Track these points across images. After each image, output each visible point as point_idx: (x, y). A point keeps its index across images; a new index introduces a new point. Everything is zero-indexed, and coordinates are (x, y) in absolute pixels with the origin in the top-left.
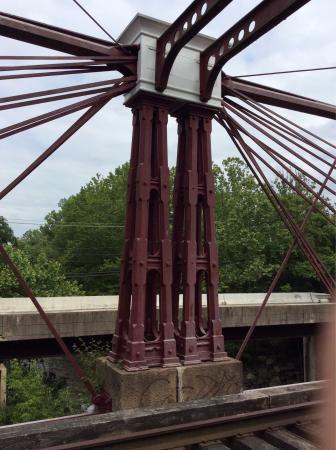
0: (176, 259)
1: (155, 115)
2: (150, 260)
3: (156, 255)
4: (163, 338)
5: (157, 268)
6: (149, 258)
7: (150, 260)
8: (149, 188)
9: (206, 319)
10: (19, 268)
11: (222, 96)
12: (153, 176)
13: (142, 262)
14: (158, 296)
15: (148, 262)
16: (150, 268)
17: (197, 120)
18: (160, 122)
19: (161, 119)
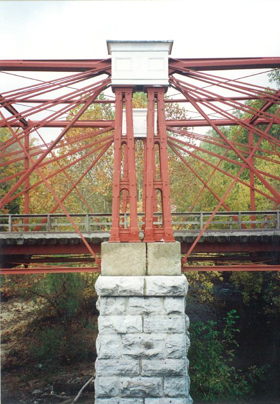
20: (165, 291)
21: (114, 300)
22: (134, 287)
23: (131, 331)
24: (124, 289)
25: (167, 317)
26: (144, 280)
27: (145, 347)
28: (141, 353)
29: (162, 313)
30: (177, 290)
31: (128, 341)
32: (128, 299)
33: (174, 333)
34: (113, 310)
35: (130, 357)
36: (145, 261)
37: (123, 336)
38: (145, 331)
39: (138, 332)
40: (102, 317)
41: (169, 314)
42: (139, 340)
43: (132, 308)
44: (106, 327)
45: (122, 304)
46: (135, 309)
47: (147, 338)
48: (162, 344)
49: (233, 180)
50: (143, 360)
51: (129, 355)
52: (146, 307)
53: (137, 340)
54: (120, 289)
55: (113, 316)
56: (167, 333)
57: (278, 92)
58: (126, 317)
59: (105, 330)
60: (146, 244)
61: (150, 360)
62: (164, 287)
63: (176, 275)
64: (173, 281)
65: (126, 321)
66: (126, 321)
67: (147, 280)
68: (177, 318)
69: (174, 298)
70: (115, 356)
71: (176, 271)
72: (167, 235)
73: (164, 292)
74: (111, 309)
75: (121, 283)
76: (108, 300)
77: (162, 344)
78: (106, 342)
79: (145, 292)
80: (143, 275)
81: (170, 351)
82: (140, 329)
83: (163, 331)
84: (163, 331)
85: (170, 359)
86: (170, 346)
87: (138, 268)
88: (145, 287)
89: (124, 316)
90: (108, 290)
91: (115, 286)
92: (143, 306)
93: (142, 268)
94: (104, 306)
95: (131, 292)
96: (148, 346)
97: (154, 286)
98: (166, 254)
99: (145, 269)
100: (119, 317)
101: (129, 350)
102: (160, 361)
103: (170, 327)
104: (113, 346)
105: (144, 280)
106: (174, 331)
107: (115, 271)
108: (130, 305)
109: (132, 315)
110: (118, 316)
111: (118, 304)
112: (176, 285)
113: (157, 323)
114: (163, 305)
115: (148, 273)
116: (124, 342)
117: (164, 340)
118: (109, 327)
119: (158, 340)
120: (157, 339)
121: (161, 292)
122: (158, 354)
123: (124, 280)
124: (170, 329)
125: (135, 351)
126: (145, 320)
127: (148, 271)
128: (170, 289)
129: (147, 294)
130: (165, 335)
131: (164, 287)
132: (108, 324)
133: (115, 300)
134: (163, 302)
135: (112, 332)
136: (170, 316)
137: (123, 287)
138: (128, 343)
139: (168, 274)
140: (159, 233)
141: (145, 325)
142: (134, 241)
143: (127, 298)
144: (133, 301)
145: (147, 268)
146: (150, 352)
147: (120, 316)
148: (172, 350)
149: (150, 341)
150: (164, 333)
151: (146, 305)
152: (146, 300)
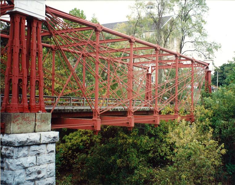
0: (19, 87)
1: (21, 20)
2: (19, 75)
3: (21, 73)
4: (24, 103)
5: (21, 78)
6: (19, 74)
7: (19, 75)
8: (19, 48)
9: (139, 145)
10: (85, 95)
11: (46, 15)
12: (20, 43)
13: (17, 75)
14: (26, 21)
15: (19, 76)
16: (20, 78)
17: (36, 23)
18: (22, 23)
19: (23, 22)
20: (50, 140)
21: (22, 149)
22: (36, 139)
23: (31, 165)
24: (31, 141)
25: (48, 155)
26: (40, 134)
27: (38, 173)
28: (36, 178)
29: (46, 153)
30: (55, 138)
31: (30, 172)
32: (30, 147)
33: (50, 163)
34: (22, 154)
35: (30, 181)
36: (34, 124)
37: (26, 169)
38: (37, 164)
39: (34, 165)
40: (16, 159)
41: (48, 153)
42: (35, 170)
43: (31, 152)
44: (17, 165)
45: (26, 150)
46: (33, 152)
47: (38, 168)
48: (45, 170)
49: (164, 110)
50: (36, 181)
51: (29, 180)
52: (39, 150)
53: (34, 170)
54: (29, 141)
55: (21, 158)
56: (48, 163)
57: (60, 30)
58: (28, 158)
59: (17, 167)
60: (35, 114)
61: (39, 180)
62: (50, 138)
63: (49, 131)
64: (54, 134)
65: (28, 160)
66: (28, 160)
67: (41, 134)
68: (52, 155)
69: (52, 144)
70: (22, 182)
71: (49, 129)
72: (42, 109)
73: (49, 140)
74: (21, 154)
75: (29, 137)
76: (19, 149)
77: (45, 170)
78: (18, 174)
79: (40, 142)
80: (33, 132)
81: (48, 173)
82: (35, 164)
83: (46, 163)
84: (46, 163)
85: (49, 178)
86: (49, 171)
87: (31, 128)
88: (40, 139)
89: (27, 157)
90: (23, 142)
91: (26, 139)
92: (38, 150)
93: (32, 130)
94: (17, 153)
95: (34, 142)
96: (39, 173)
97: (45, 138)
98: (44, 121)
99: (34, 129)
100: (25, 158)
101: (29, 177)
102: (44, 180)
103: (49, 160)
104: (22, 176)
105: (40, 134)
106: (51, 162)
107: (19, 131)
108: (31, 150)
109: (31, 156)
110: (24, 158)
111: (24, 151)
112: (56, 136)
113: (43, 159)
114: (46, 148)
115: (36, 131)
116: (27, 173)
117: (46, 168)
118: (20, 165)
119: (44, 168)
120: (43, 168)
121: (47, 141)
122: (44, 176)
123: (30, 135)
124: (49, 161)
125: (33, 177)
126: (37, 158)
127: (36, 129)
128: (52, 138)
129: (41, 143)
130: (47, 165)
131: (50, 138)
132: (20, 163)
133: (23, 148)
134: (47, 146)
135: (20, 168)
136: (50, 154)
137: (30, 140)
138: (29, 173)
139: (45, 131)
140: (38, 107)
141: (37, 161)
142: (27, 112)
143: (29, 146)
144: (33, 148)
145: (35, 128)
146: (40, 176)
147: (25, 158)
148: (50, 172)
149: (40, 170)
150: (46, 164)
151: (39, 149)
152: (39, 146)
